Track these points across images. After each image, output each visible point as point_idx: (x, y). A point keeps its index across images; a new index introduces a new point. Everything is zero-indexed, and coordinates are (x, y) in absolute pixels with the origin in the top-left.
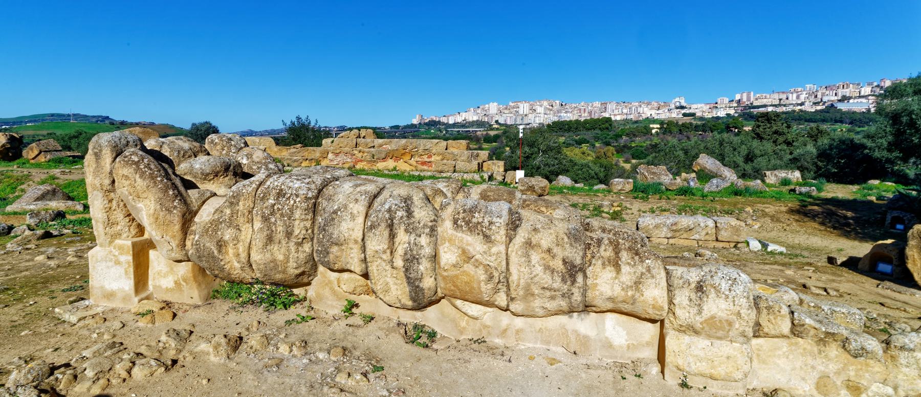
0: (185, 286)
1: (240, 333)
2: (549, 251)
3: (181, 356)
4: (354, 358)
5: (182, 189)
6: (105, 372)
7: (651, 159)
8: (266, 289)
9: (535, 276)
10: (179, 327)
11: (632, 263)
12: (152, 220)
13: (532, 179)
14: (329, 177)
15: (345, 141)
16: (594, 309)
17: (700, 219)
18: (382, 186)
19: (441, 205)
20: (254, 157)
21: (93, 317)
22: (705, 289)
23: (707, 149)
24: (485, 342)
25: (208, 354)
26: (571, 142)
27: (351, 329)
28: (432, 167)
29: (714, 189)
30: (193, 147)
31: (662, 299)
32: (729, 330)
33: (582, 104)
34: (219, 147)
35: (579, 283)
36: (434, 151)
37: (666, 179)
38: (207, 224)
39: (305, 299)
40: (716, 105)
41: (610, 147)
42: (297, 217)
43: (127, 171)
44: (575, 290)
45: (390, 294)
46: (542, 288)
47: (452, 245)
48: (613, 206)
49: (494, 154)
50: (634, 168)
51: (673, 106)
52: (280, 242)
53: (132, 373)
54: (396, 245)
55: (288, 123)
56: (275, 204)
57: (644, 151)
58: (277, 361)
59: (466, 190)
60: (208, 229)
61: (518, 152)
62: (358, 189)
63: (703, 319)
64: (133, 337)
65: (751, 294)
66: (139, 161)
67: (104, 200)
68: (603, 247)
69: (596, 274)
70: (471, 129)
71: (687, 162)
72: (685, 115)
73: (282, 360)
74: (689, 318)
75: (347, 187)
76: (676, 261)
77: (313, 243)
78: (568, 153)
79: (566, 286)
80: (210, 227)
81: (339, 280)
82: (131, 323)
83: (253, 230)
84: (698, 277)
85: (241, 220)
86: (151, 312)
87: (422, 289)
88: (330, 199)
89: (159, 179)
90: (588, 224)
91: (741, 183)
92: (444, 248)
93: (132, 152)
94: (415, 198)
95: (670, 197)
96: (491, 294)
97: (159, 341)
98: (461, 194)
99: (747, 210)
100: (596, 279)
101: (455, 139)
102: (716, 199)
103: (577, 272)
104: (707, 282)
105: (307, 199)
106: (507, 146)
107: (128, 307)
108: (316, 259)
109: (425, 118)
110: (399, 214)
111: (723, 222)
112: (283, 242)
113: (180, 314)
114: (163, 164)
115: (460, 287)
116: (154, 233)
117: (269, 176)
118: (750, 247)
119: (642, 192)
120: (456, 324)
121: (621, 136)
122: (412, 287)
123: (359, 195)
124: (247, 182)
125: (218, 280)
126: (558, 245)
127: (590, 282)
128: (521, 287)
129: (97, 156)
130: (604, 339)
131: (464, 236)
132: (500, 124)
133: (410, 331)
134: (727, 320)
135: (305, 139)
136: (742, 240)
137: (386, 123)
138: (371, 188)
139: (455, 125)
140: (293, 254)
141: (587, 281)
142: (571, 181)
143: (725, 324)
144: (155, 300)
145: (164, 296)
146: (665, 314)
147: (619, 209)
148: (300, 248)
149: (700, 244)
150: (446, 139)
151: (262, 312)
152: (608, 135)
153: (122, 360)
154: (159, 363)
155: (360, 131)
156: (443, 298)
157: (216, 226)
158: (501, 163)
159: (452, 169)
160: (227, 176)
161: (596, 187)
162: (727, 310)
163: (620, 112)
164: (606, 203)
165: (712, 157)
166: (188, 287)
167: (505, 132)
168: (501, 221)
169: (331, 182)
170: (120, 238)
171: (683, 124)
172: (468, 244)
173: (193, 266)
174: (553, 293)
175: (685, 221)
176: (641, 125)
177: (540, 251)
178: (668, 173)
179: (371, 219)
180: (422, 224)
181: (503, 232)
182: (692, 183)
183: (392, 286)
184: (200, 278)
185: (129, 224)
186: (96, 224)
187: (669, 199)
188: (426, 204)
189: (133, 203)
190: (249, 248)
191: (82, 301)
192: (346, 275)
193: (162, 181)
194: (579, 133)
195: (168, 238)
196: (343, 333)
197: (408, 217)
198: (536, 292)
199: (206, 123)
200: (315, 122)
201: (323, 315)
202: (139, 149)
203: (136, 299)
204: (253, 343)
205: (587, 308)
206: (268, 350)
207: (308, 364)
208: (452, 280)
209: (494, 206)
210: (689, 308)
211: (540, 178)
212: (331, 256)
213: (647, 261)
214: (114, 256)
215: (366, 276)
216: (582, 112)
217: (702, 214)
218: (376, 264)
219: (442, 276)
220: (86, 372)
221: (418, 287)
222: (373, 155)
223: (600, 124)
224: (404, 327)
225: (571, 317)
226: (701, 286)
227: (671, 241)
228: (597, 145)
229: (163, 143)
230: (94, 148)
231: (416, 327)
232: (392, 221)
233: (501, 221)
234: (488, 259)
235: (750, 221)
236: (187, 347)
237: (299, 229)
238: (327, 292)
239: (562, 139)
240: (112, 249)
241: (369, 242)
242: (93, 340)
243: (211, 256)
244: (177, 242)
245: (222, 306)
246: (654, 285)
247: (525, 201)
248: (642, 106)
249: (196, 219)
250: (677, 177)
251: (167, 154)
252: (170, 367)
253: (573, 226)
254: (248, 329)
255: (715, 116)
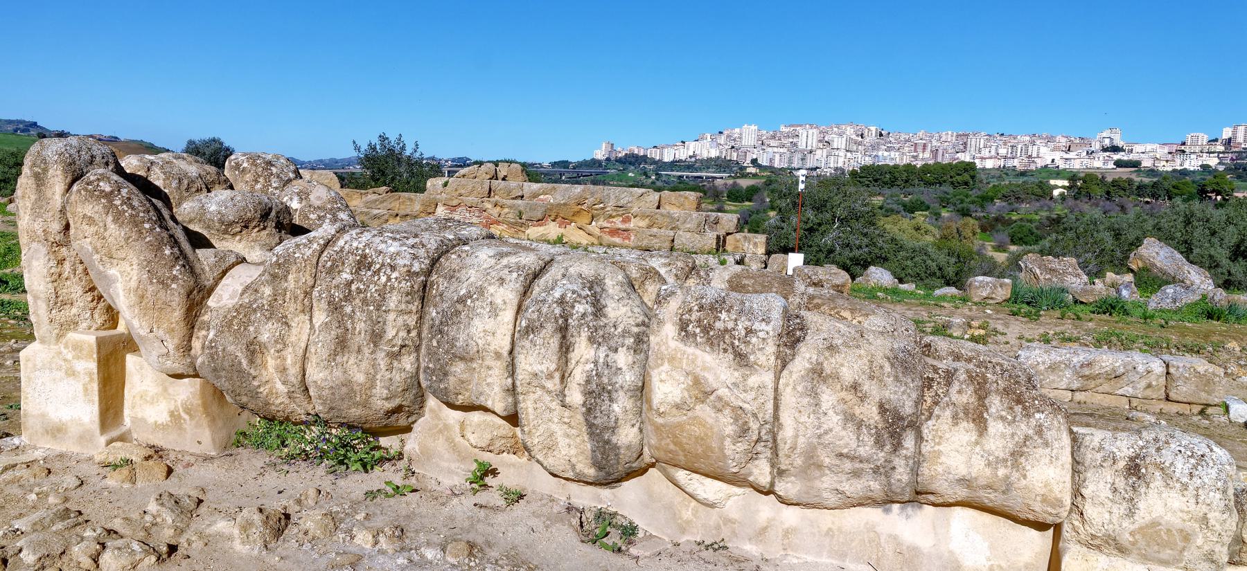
0: (188, 422)
1: (285, 508)
2: (855, 388)
3: (183, 541)
4: (489, 561)
5: (186, 246)
6: (54, 557)
7: (1048, 245)
8: (330, 434)
9: (826, 433)
10: (179, 492)
11: (1010, 418)
12: (133, 298)
13: (819, 270)
14: (451, 237)
15: (467, 185)
16: (931, 498)
17: (1139, 359)
18: (547, 258)
19: (658, 295)
20: (312, 197)
21: (28, 466)
22: (1143, 471)
23: (1159, 229)
24: (725, 548)
25: (230, 538)
26: (895, 207)
27: (482, 513)
28: (629, 239)
29: (1167, 304)
30: (204, 173)
31: (1061, 485)
32: (1184, 549)
33: (921, 134)
34: (248, 177)
35: (907, 449)
36: (635, 210)
37: (1076, 281)
38: (229, 311)
39: (400, 456)
40: (1183, 148)
41: (970, 218)
42: (392, 305)
43: (89, 209)
44: (899, 462)
45: (555, 453)
46: (836, 455)
47: (674, 368)
48: (970, 327)
49: (746, 223)
50: (1014, 263)
51: (1096, 146)
52: (359, 351)
53: (101, 561)
54: (571, 366)
55: (364, 147)
56: (352, 282)
57: (1035, 231)
58: (352, 559)
59: (702, 273)
60: (231, 321)
61: (794, 220)
62: (505, 261)
63: (1136, 526)
64: (98, 503)
65: (1230, 484)
66: (112, 192)
67: (49, 260)
68: (956, 387)
69: (940, 434)
70: (704, 174)
71: (1118, 254)
72: (1119, 164)
73: (360, 558)
74: (1111, 522)
75: (485, 255)
76: (1091, 420)
77: (418, 356)
78: (888, 227)
79: (883, 454)
80: (235, 317)
81: (462, 425)
82: (95, 480)
83: (312, 327)
84: (1132, 450)
85: (291, 307)
86: (128, 462)
87: (616, 447)
88: (452, 277)
89: (147, 226)
90: (928, 346)
91: (1221, 297)
92: (660, 374)
93: (100, 175)
94: (609, 282)
95: (1081, 315)
96: (743, 461)
97: (145, 512)
98: (692, 280)
99: (1229, 345)
100: (939, 444)
101: (673, 190)
102: (1171, 323)
103: (904, 429)
104: (1148, 460)
105: (411, 274)
106: (773, 208)
107: (88, 452)
108: (424, 384)
109: (619, 149)
110: (580, 308)
111: (1181, 365)
112: (366, 351)
113: (178, 469)
114: (153, 200)
115: (687, 447)
116: (136, 323)
117: (342, 231)
118: (1231, 416)
119: (1028, 303)
120: (675, 514)
121: (992, 200)
122: (598, 442)
123: (506, 271)
124: (302, 239)
125: (246, 413)
126: (871, 378)
127: (928, 448)
128: (798, 451)
129: (40, 179)
130: (947, 554)
131: (698, 352)
132: (760, 166)
133: (589, 523)
134: (1182, 531)
135: (393, 179)
136: (1217, 401)
137: (545, 158)
138: (529, 260)
139: (675, 164)
140: (383, 374)
141: (922, 447)
142: (892, 277)
143: (1178, 537)
144: (135, 442)
145: (151, 437)
146: (1065, 514)
147: (982, 332)
148: (395, 364)
149: (1134, 404)
150: (659, 190)
151: (323, 474)
152: (967, 196)
153: (82, 539)
154: (147, 547)
155: (497, 166)
156: (653, 465)
157: (245, 316)
158: (761, 239)
159: (668, 244)
160: (265, 228)
161: (938, 292)
162: (1182, 511)
163: (993, 153)
164: (957, 320)
165: (1170, 245)
166: (194, 422)
167: (769, 183)
168: (769, 328)
169: (454, 246)
170: (75, 330)
171: (1114, 181)
172: (704, 368)
173: (203, 387)
174: (858, 465)
175: (1109, 360)
176: (1032, 179)
177: (839, 387)
178: (1080, 271)
179: (528, 315)
180: (620, 330)
181: (771, 349)
182: (1125, 293)
183: (560, 439)
184: (215, 408)
185: (92, 305)
186: (35, 302)
187: (1079, 318)
188: (628, 294)
189: (101, 268)
190: (304, 358)
191: (8, 439)
192: (476, 416)
193: (152, 229)
194: (911, 189)
195: (161, 333)
196: (468, 518)
197: (595, 315)
198: (827, 461)
199: (214, 140)
200: (414, 146)
201: (432, 485)
202: (112, 171)
203: (103, 440)
204: (309, 525)
205: (919, 495)
206: (335, 538)
207: (407, 567)
208: (673, 432)
209: (757, 302)
210: (1110, 504)
211: (834, 269)
212: (452, 379)
213: (1037, 416)
214: (65, 360)
215: (513, 419)
216: (920, 149)
217: (1141, 350)
218: (532, 397)
219: (653, 424)
220: (21, 555)
221: (608, 442)
222: (520, 213)
223: (952, 174)
224: (579, 515)
225: (887, 511)
226: (1137, 466)
227: (1079, 396)
228: (945, 214)
229: (152, 163)
230: (34, 165)
231: (600, 515)
232: (567, 320)
233: (769, 328)
234: (742, 396)
235: (1233, 368)
236: (193, 526)
237: (394, 329)
238: (440, 445)
239: (878, 200)
240: (62, 349)
241: (523, 356)
242: (30, 504)
243: (236, 368)
244: (176, 341)
245: (252, 460)
246: (1047, 460)
247: (811, 298)
248: (1038, 142)
249: (211, 302)
250: (1097, 281)
251: (159, 183)
252: (165, 556)
253: (902, 345)
254: (299, 502)
255: (1179, 168)
